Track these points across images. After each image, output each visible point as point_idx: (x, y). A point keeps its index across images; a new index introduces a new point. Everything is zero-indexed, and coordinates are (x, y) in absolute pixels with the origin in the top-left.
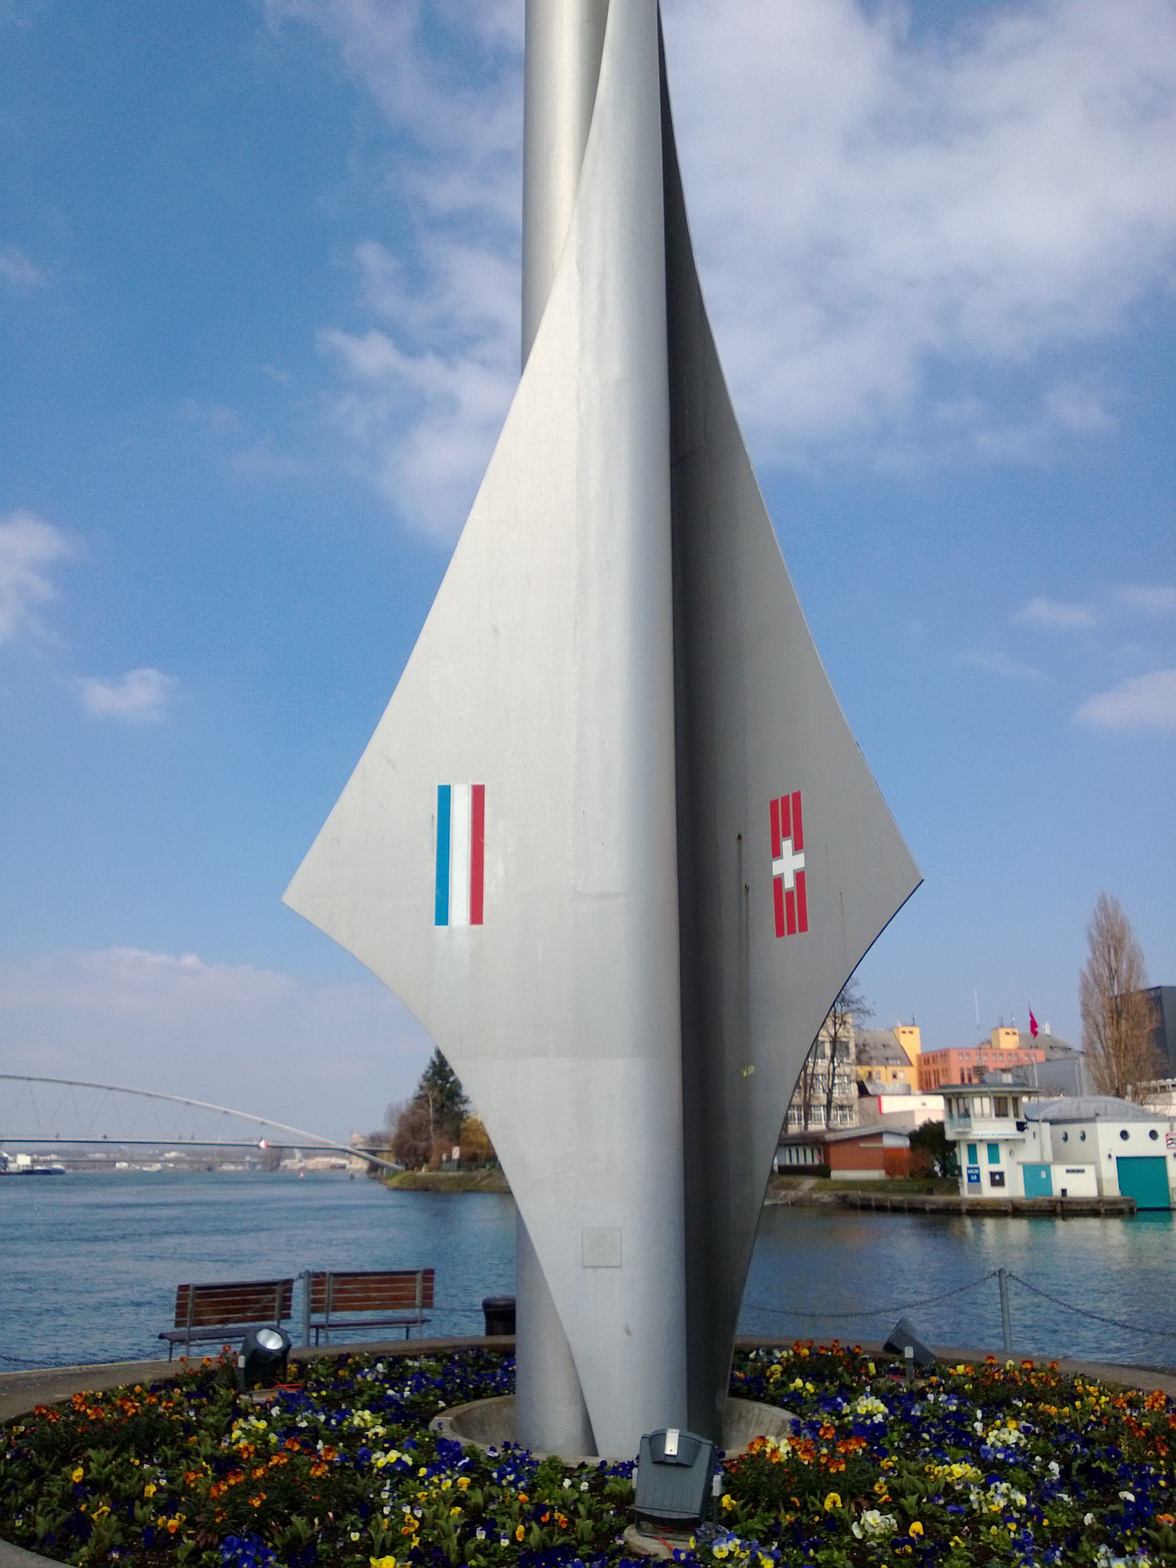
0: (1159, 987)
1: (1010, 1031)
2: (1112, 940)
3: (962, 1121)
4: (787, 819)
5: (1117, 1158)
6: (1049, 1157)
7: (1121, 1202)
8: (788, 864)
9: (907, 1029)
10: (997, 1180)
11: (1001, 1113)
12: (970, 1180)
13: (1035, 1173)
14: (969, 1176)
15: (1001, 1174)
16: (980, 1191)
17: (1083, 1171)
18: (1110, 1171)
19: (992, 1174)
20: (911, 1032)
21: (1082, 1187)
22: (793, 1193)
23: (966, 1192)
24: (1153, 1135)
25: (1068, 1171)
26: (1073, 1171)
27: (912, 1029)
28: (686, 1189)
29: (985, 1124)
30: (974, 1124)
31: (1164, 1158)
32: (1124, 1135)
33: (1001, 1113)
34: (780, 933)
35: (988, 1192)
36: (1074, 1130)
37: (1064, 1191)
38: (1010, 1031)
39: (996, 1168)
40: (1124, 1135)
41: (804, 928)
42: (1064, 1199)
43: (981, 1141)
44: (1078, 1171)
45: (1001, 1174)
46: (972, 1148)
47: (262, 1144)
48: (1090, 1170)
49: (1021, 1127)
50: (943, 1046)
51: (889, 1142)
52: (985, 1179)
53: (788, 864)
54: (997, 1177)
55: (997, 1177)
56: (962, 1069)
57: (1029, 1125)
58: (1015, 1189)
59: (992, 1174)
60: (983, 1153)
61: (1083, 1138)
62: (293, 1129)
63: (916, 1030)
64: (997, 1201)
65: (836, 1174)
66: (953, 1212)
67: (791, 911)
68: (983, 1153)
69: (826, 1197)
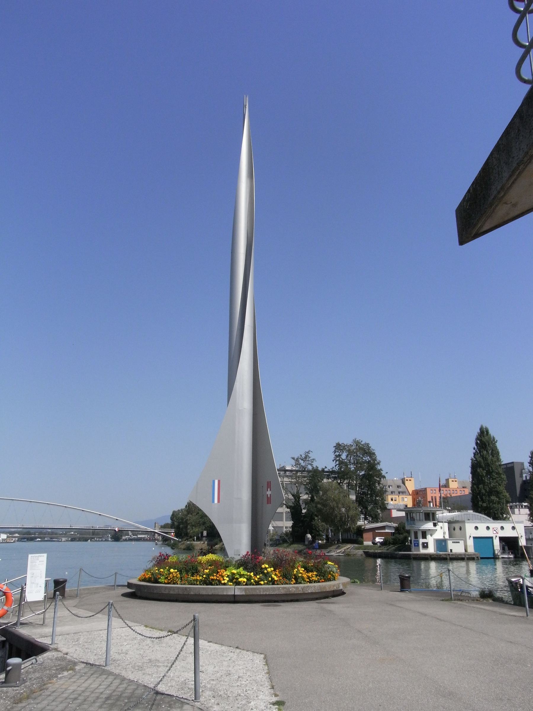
0: (513, 463)
1: (454, 480)
2: (485, 443)
3: (412, 522)
4: (269, 485)
5: (474, 538)
6: (447, 537)
7: (474, 554)
8: (269, 493)
9: (408, 479)
10: (425, 546)
12: (415, 546)
14: (414, 544)
15: (427, 543)
16: (419, 550)
17: (459, 542)
18: (470, 543)
20: (410, 480)
21: (457, 548)
24: (488, 528)
25: (453, 542)
26: (455, 542)
28: (252, 543)
30: (416, 523)
31: (492, 538)
32: (476, 528)
35: (423, 551)
36: (457, 526)
37: (451, 550)
38: (454, 480)
39: (424, 541)
40: (476, 528)
44: (457, 542)
48: (462, 542)
49: (435, 525)
50: (423, 487)
53: (269, 493)
56: (432, 497)
59: (423, 543)
61: (460, 529)
64: (425, 555)
67: (269, 500)
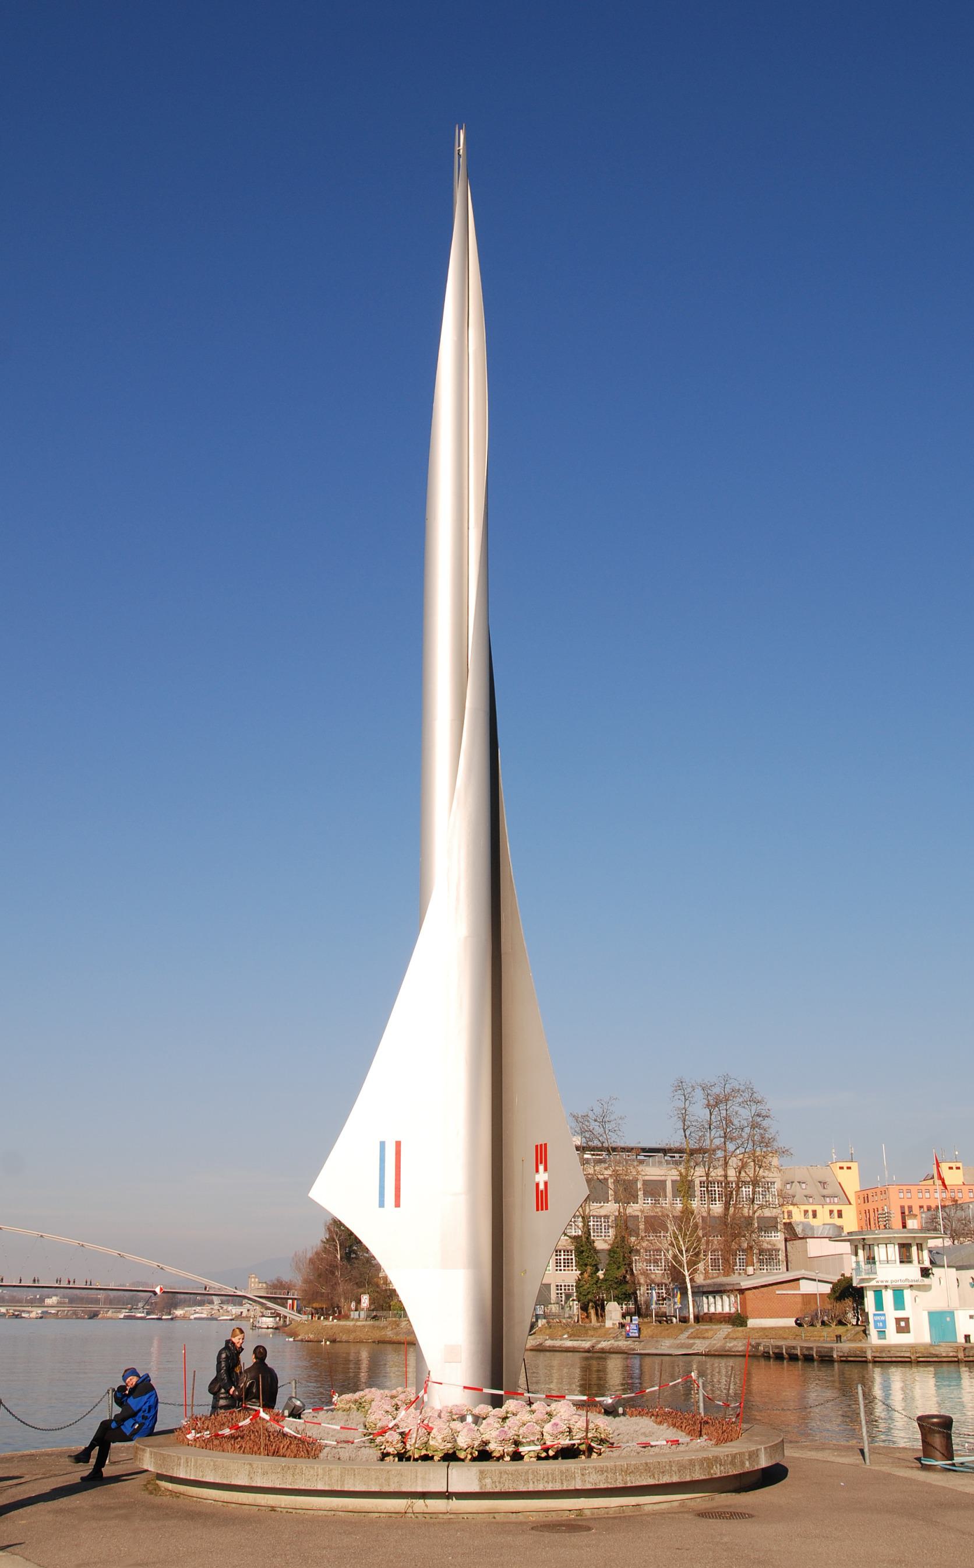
9: (845, 1165)
11: (905, 1259)
13: (941, 1320)
14: (875, 1322)
15: (907, 1320)
19: (898, 1320)
22: (707, 1342)
23: (874, 1339)
27: (849, 1164)
29: (890, 1270)
30: (878, 1270)
33: (905, 1259)
34: (538, 1210)
35: (894, 1338)
39: (901, 1314)
41: (547, 1209)
42: (968, 1345)
43: (886, 1287)
45: (907, 1320)
46: (878, 1293)
47: (158, 1290)
51: (807, 1287)
52: (891, 1326)
54: (903, 1324)
55: (903, 1324)
57: (935, 1270)
58: (920, 1335)
59: (898, 1320)
60: (888, 1296)
62: (101, 1249)
63: (854, 1166)
65: (752, 1323)
66: (859, 1362)
68: (888, 1296)
69: (739, 1346)
